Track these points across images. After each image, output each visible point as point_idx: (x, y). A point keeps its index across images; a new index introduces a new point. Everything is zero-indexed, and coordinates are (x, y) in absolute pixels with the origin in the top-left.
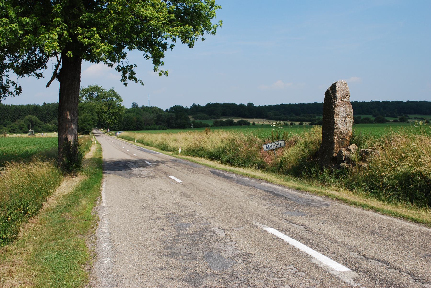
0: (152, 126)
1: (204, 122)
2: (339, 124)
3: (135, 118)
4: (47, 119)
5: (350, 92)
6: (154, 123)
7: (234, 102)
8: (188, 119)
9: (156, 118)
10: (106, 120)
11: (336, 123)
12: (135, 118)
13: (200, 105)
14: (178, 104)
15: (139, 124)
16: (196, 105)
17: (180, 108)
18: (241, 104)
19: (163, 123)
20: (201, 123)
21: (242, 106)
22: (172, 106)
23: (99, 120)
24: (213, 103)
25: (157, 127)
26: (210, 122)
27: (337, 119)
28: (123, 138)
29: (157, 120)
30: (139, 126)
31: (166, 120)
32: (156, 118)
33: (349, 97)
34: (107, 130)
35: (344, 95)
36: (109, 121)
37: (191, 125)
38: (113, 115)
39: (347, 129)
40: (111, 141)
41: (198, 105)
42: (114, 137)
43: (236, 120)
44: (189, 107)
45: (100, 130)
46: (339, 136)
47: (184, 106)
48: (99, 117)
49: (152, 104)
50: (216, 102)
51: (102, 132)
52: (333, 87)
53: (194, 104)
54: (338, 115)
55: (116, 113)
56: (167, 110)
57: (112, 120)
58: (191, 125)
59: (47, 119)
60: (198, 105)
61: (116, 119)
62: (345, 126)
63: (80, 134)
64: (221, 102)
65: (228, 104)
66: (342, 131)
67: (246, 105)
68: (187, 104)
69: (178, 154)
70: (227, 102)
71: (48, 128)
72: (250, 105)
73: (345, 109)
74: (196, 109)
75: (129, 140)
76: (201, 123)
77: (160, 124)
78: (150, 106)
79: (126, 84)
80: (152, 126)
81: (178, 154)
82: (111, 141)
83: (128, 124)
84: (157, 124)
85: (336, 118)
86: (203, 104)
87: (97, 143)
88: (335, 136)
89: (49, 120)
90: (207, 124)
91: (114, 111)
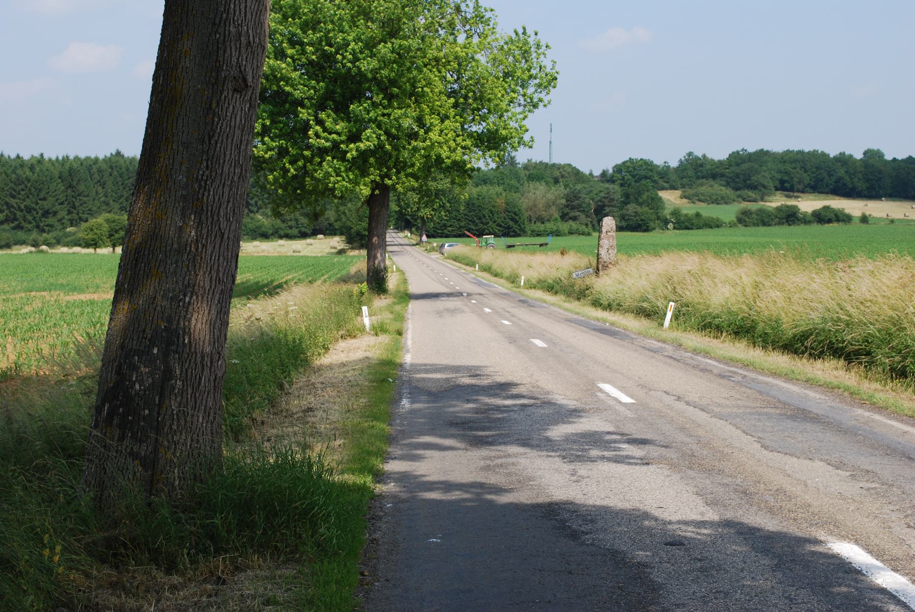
0: (549, 226)
1: (708, 211)
3: (501, 202)
4: (252, 202)
6: (557, 215)
7: (820, 148)
8: (656, 203)
9: (564, 201)
10: (419, 209)
12: (501, 202)
13: (710, 156)
14: (637, 155)
15: (512, 219)
16: (697, 158)
17: (647, 165)
18: (842, 154)
19: (583, 216)
20: (698, 215)
21: (843, 160)
22: (620, 162)
23: (400, 212)
24: (752, 149)
25: (564, 227)
26: (728, 212)
28: (456, 259)
29: (567, 206)
30: (511, 223)
31: (593, 206)
32: (564, 201)
34: (421, 236)
36: (426, 212)
37: (666, 222)
38: (437, 196)
40: (423, 264)
41: (704, 156)
42: (435, 255)
43: (808, 204)
44: (674, 164)
45: (401, 235)
47: (658, 161)
48: (400, 206)
49: (560, 159)
50: (759, 148)
51: (406, 241)
53: (690, 154)
55: (443, 192)
56: (604, 174)
57: (434, 210)
58: (666, 222)
59: (252, 202)
60: (704, 156)
61: (443, 206)
63: (352, 248)
64: (777, 146)
65: (801, 152)
67: (858, 155)
68: (667, 154)
69: (519, 287)
70: (795, 147)
71: (259, 227)
72: (872, 155)
74: (695, 173)
75: (467, 265)
76: (698, 215)
77: (574, 219)
78: (552, 162)
79: (524, 28)
80: (549, 226)
81: (519, 287)
82: (428, 267)
83: (480, 219)
84: (564, 217)
86: (719, 153)
87: (398, 270)
89: (260, 203)
90: (718, 220)
91: (440, 187)
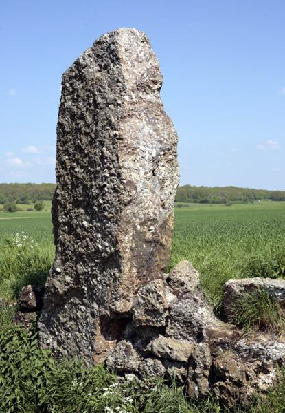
2: (140, 186)
5: (162, 71)
11: (130, 183)
27: (131, 164)
33: (159, 89)
35: (147, 79)
39: (163, 206)
46: (139, 233)
52: (107, 53)
54: (132, 150)
62: (158, 192)
66: (150, 211)
73: (156, 130)
85: (127, 162)
88: (126, 233)
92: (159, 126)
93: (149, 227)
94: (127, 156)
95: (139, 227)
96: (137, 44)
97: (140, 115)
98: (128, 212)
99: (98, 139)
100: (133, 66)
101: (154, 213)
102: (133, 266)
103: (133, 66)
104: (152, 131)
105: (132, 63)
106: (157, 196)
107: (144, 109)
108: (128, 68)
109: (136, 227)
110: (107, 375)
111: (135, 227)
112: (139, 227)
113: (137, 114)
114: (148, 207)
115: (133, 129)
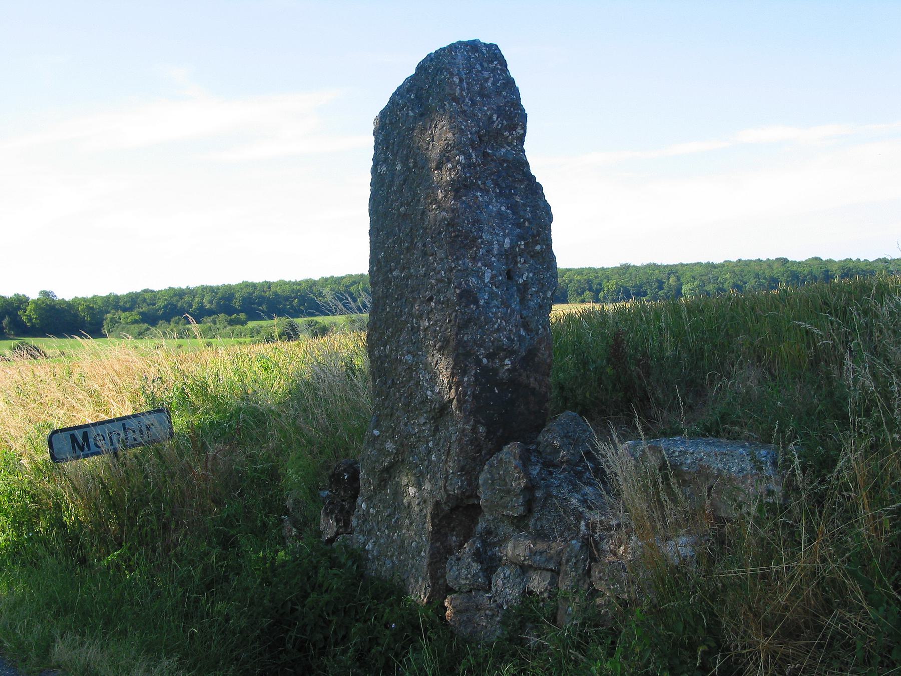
46: (485, 370)
92: (518, 199)
93: (502, 360)
94: (462, 251)
95: (485, 361)
96: (481, 65)
97: (484, 184)
98: (465, 338)
99: (140, 439)
100: (474, 103)
101: (509, 338)
102: (477, 422)
103: (474, 103)
104: (503, 208)
105: (471, 99)
106: (513, 311)
107: (492, 174)
108: (466, 108)
109: (481, 360)
110: (153, 369)
111: (478, 362)
112: (485, 361)
113: (480, 182)
114: (498, 330)
115: (470, 207)
